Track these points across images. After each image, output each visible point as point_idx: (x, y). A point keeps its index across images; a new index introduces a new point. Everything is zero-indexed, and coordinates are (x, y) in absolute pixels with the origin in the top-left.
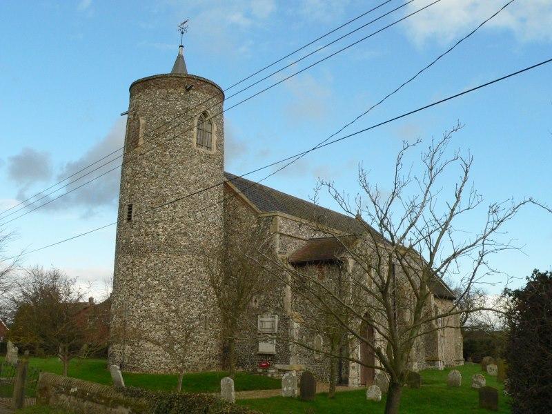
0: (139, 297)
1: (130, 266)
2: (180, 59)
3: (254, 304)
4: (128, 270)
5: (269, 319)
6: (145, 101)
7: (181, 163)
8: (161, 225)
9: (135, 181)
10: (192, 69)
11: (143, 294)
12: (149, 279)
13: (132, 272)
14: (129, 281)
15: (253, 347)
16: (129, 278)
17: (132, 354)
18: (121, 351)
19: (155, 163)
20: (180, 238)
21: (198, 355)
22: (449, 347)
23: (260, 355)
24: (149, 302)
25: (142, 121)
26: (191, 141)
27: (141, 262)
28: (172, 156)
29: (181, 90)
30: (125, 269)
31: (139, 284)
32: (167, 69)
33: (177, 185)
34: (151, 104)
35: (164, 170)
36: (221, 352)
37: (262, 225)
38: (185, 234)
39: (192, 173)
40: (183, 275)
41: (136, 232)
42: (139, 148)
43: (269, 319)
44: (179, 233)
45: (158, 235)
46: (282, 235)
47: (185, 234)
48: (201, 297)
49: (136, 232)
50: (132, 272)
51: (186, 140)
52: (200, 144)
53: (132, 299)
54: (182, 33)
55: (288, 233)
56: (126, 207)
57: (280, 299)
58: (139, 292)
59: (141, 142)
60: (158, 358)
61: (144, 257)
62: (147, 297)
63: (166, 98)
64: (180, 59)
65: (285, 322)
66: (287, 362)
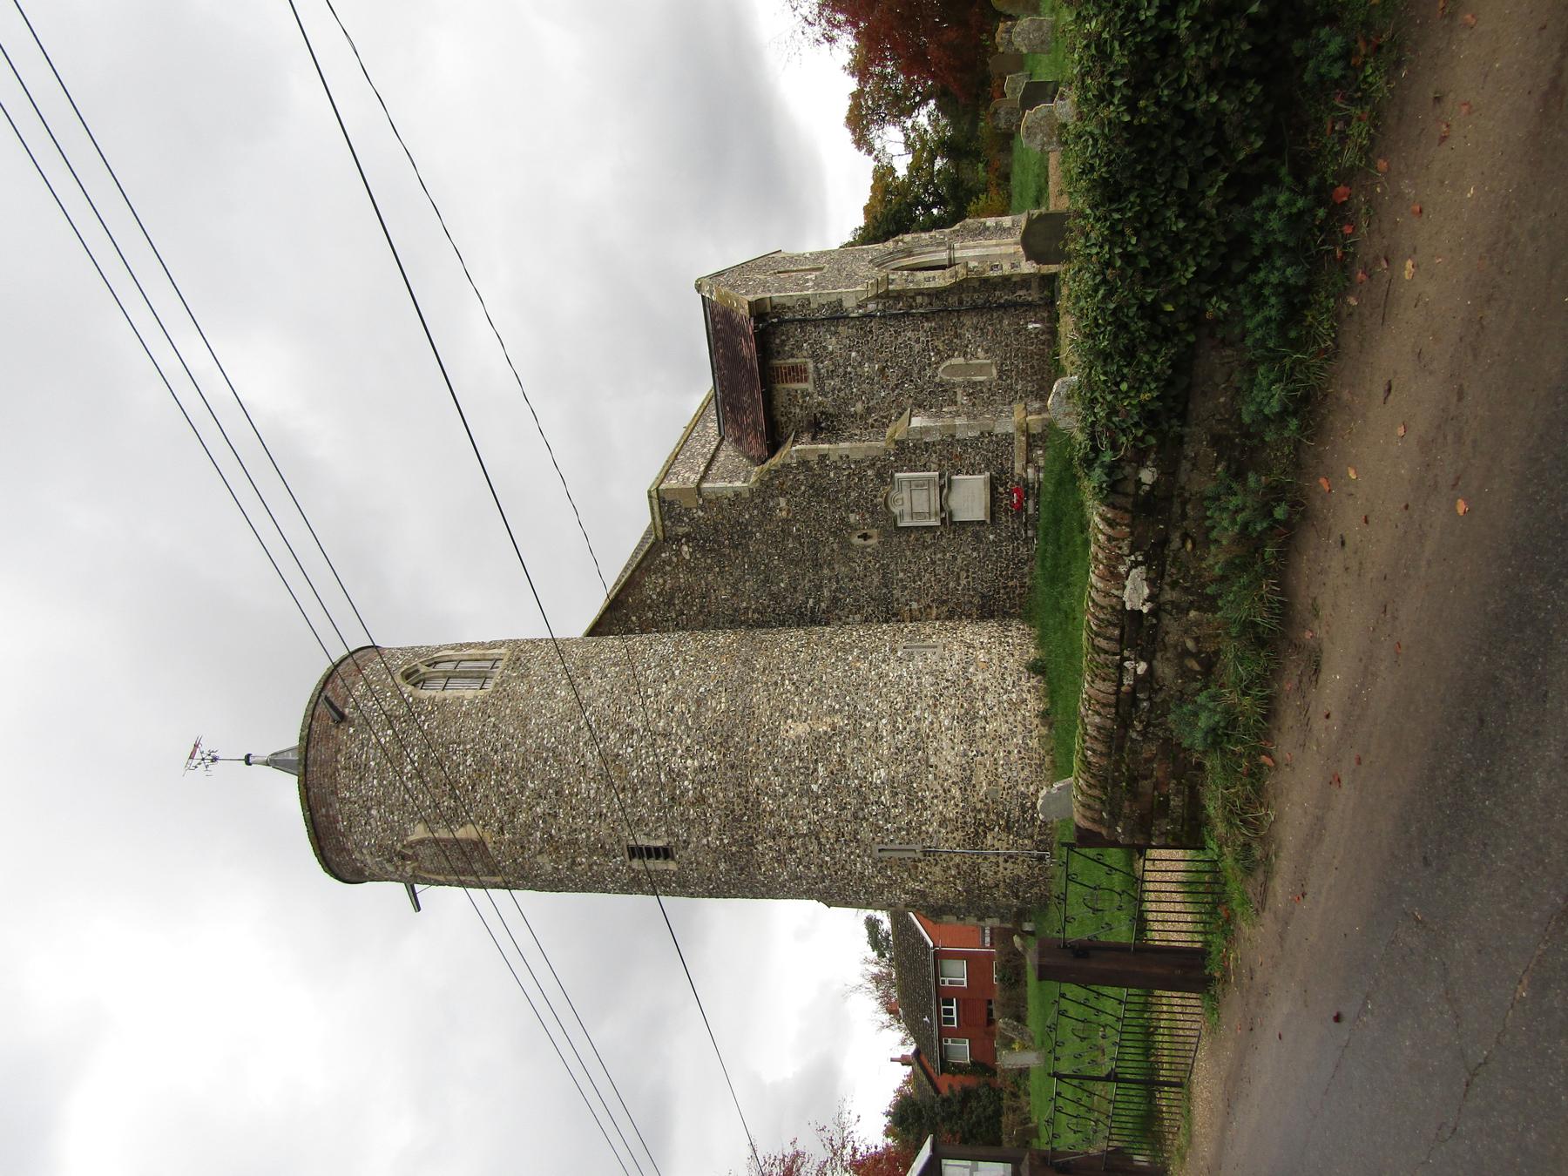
0: (861, 815)
1: (782, 841)
2: (275, 762)
3: (870, 542)
4: (792, 850)
5: (905, 495)
6: (363, 841)
7: (525, 720)
8: (676, 763)
9: (569, 842)
10: (289, 738)
11: (853, 801)
12: (815, 787)
13: (798, 836)
14: (820, 843)
15: (976, 536)
16: (814, 847)
17: (1008, 828)
18: (1001, 860)
19: (523, 788)
20: (709, 714)
21: (1001, 659)
22: (949, 208)
23: (993, 514)
24: (873, 787)
25: (419, 832)
26: (471, 702)
27: (772, 813)
28: (506, 746)
29: (346, 733)
30: (791, 858)
31: (828, 816)
32: (288, 786)
33: (579, 729)
34: (374, 812)
35: (540, 765)
36: (992, 623)
37: (681, 530)
38: (698, 702)
39: (551, 695)
40: (802, 702)
41: (697, 830)
42: (487, 837)
43: (905, 495)
44: (696, 717)
45: (701, 769)
46: (703, 478)
47: (699, 702)
48: (858, 659)
49: (697, 830)
50: (798, 836)
51: (467, 714)
52: (483, 677)
53: (865, 833)
54: (215, 759)
55: (702, 469)
56: (636, 864)
57: (857, 468)
58: (848, 814)
59: (465, 832)
60: (1015, 755)
61: (759, 803)
62: (858, 789)
63: (360, 770)
64: (275, 762)
65: (909, 453)
66: (952, 1014)
